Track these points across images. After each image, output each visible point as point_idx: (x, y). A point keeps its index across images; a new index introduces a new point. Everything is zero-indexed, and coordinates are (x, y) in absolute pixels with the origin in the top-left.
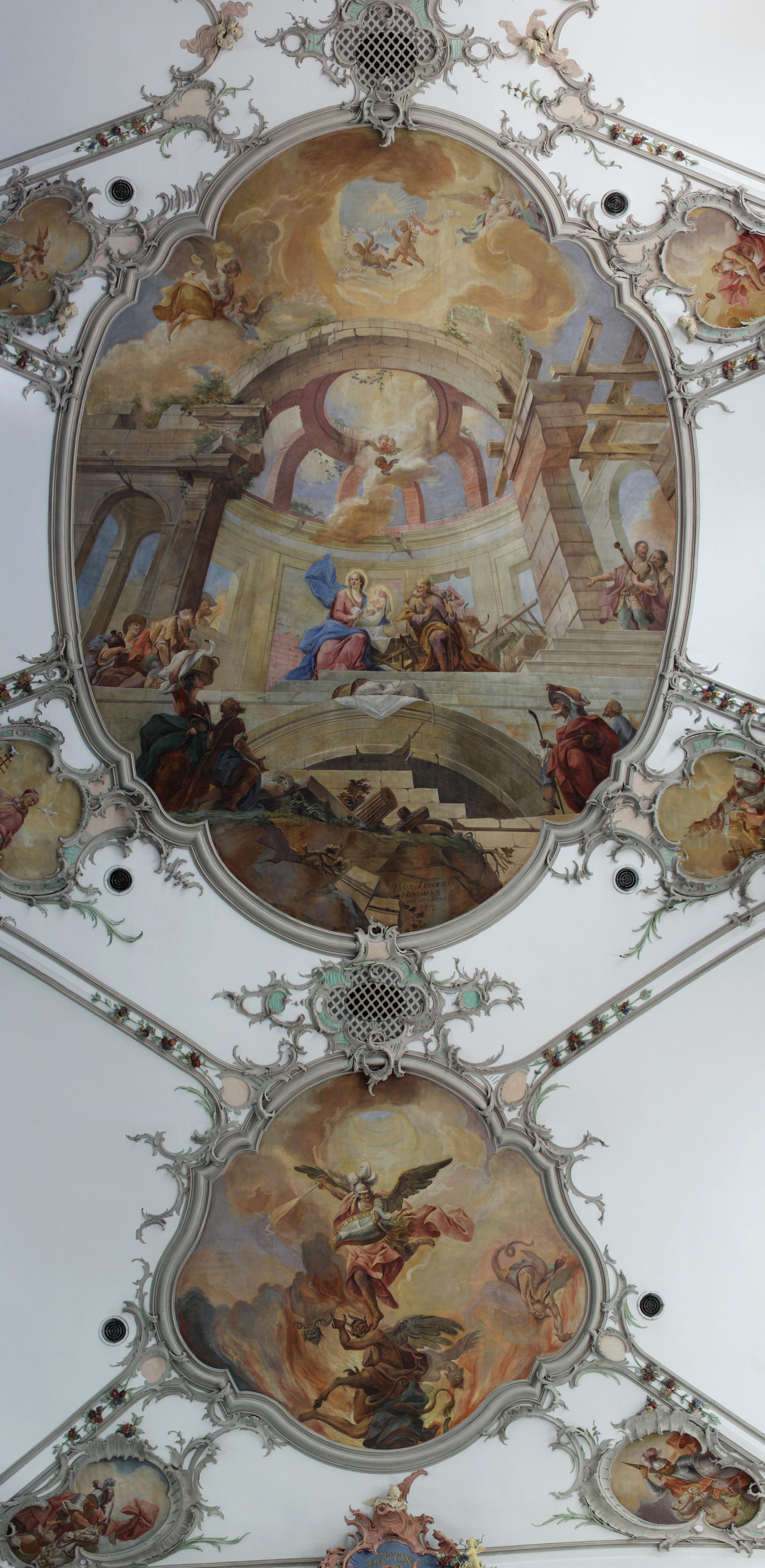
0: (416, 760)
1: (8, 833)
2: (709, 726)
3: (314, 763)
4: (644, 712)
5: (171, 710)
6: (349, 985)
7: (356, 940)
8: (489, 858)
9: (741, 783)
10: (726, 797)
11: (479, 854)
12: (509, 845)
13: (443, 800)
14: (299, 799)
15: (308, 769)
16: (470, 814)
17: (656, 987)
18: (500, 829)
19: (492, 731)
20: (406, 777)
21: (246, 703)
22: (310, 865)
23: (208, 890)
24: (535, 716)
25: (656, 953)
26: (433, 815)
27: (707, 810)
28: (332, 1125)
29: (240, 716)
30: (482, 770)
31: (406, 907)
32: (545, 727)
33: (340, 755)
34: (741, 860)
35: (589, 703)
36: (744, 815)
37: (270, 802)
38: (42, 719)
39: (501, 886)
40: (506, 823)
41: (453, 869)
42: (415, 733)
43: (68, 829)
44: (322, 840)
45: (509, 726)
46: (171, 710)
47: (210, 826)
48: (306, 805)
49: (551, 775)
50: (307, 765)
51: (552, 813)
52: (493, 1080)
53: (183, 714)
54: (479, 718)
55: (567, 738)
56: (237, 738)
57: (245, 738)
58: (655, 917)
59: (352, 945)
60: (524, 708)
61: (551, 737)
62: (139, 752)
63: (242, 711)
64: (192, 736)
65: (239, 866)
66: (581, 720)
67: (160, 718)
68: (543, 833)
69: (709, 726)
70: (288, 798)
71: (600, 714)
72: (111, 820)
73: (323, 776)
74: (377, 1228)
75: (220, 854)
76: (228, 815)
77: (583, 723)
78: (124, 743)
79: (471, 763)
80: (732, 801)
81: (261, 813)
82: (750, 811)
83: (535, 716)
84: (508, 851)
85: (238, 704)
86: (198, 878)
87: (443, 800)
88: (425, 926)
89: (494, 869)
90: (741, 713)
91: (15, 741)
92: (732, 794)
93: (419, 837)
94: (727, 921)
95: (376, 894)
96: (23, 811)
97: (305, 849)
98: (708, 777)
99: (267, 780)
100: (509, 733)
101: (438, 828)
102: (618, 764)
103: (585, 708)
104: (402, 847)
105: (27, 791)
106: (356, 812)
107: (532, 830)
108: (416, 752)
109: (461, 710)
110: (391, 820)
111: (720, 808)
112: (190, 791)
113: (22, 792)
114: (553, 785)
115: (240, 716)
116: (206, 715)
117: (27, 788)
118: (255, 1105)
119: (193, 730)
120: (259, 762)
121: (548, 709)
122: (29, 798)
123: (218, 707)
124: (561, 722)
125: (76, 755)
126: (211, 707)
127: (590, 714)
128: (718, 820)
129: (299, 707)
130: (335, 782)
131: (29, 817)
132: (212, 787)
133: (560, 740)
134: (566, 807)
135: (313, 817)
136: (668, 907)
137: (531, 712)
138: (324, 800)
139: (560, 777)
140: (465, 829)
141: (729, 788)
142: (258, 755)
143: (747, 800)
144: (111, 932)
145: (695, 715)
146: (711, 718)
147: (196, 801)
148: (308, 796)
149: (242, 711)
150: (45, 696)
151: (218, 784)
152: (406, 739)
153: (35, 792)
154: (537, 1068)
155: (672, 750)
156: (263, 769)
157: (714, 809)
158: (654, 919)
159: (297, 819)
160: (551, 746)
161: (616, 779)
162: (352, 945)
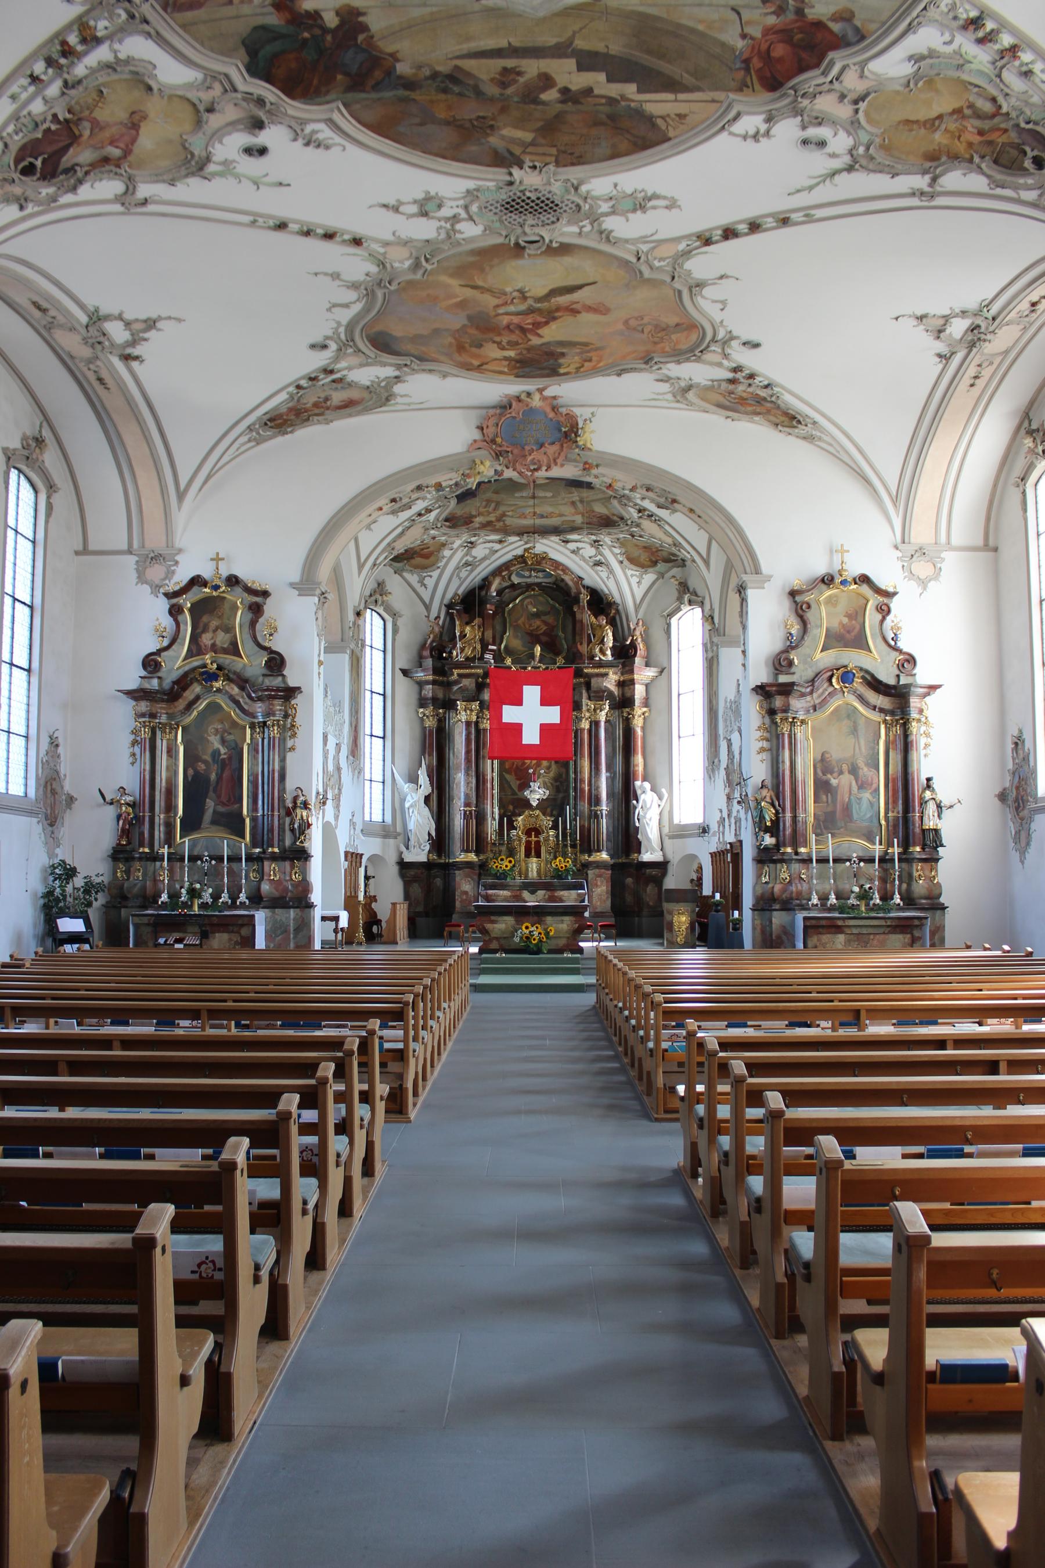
0: (581, 51)
1: (127, 146)
2: (958, 53)
3: (458, 54)
4: (884, 23)
5: (274, 19)
6: (504, 197)
7: (511, 174)
8: (659, 121)
9: (971, 106)
10: (950, 110)
11: (650, 120)
12: (683, 112)
13: (609, 80)
14: (443, 82)
15: (451, 59)
16: (640, 91)
17: (819, 213)
18: (676, 100)
19: (679, 26)
20: (571, 63)
21: (368, 8)
22: (461, 127)
23: (351, 148)
24: (739, 14)
25: (825, 193)
26: (596, 92)
27: (923, 114)
28: (492, 267)
29: (361, 19)
30: (662, 56)
31: (564, 152)
32: (748, 23)
33: (489, 48)
34: (944, 159)
35: (813, 7)
36: (962, 130)
37: (410, 84)
38: (122, 56)
39: (669, 139)
40: (681, 96)
41: (617, 128)
42: (581, 29)
43: (188, 127)
44: (470, 110)
45: (701, 21)
46: (274, 19)
47: (345, 105)
48: (451, 86)
49: (747, 62)
50: (450, 56)
51: (741, 90)
52: (644, 248)
53: (290, 22)
54: (665, 16)
55: (774, 33)
56: (361, 38)
57: (372, 37)
58: (834, 174)
59: (508, 178)
60: (725, 6)
61: (756, 32)
62: (246, 59)
63: (364, 14)
64: (305, 41)
65: (381, 128)
66: (796, 21)
67: (263, 28)
68: (725, 105)
69: (958, 53)
70: (430, 82)
71: (824, 19)
72: (230, 112)
73: (469, 65)
74: (529, 309)
75: (360, 122)
76: (363, 95)
77: (798, 24)
78: (226, 53)
79: (649, 52)
80: (955, 117)
81: (401, 92)
82: (970, 129)
83: (739, 14)
84: (681, 117)
85: (357, 9)
86: (338, 139)
87: (609, 80)
88: (583, 163)
89: (664, 128)
90: (1002, 54)
91: (104, 85)
92: (958, 112)
93: (579, 107)
94: (910, 191)
95: (533, 144)
96: (135, 127)
97: (454, 116)
98: (937, 91)
99: (403, 68)
100: (701, 27)
101: (603, 101)
102: (832, 64)
103: (806, 11)
104: (559, 117)
105: (133, 113)
106: (509, 91)
107: (713, 101)
108: (580, 44)
109: (641, 9)
110: (550, 95)
111: (940, 117)
112: (315, 82)
113: (128, 115)
114: (747, 70)
115: (361, 19)
116: (319, 21)
117: (130, 111)
118: (417, 258)
119: (306, 35)
120: (393, 55)
121: (757, 8)
122: (136, 117)
123: (332, 14)
124: (772, 20)
125: (172, 73)
126: (323, 14)
127: (810, 17)
128: (933, 125)
129: (434, 9)
130: (485, 70)
131: (142, 131)
132: (339, 77)
133: (763, 36)
134: (757, 86)
135: (460, 94)
136: (850, 169)
137: (733, 9)
138: (471, 82)
139: (756, 63)
140: (633, 101)
141: (957, 105)
142: (390, 49)
143: (972, 121)
144: (257, 184)
145: (947, 37)
146: (965, 44)
147: (323, 89)
148: (452, 81)
149: (364, 14)
150: (118, 34)
151: (347, 74)
152: (570, 33)
153: (141, 111)
154: (689, 243)
155: (903, 61)
156: (398, 60)
157: (934, 114)
158: (834, 174)
159: (443, 96)
160: (752, 38)
161: (825, 73)
162: (508, 178)
